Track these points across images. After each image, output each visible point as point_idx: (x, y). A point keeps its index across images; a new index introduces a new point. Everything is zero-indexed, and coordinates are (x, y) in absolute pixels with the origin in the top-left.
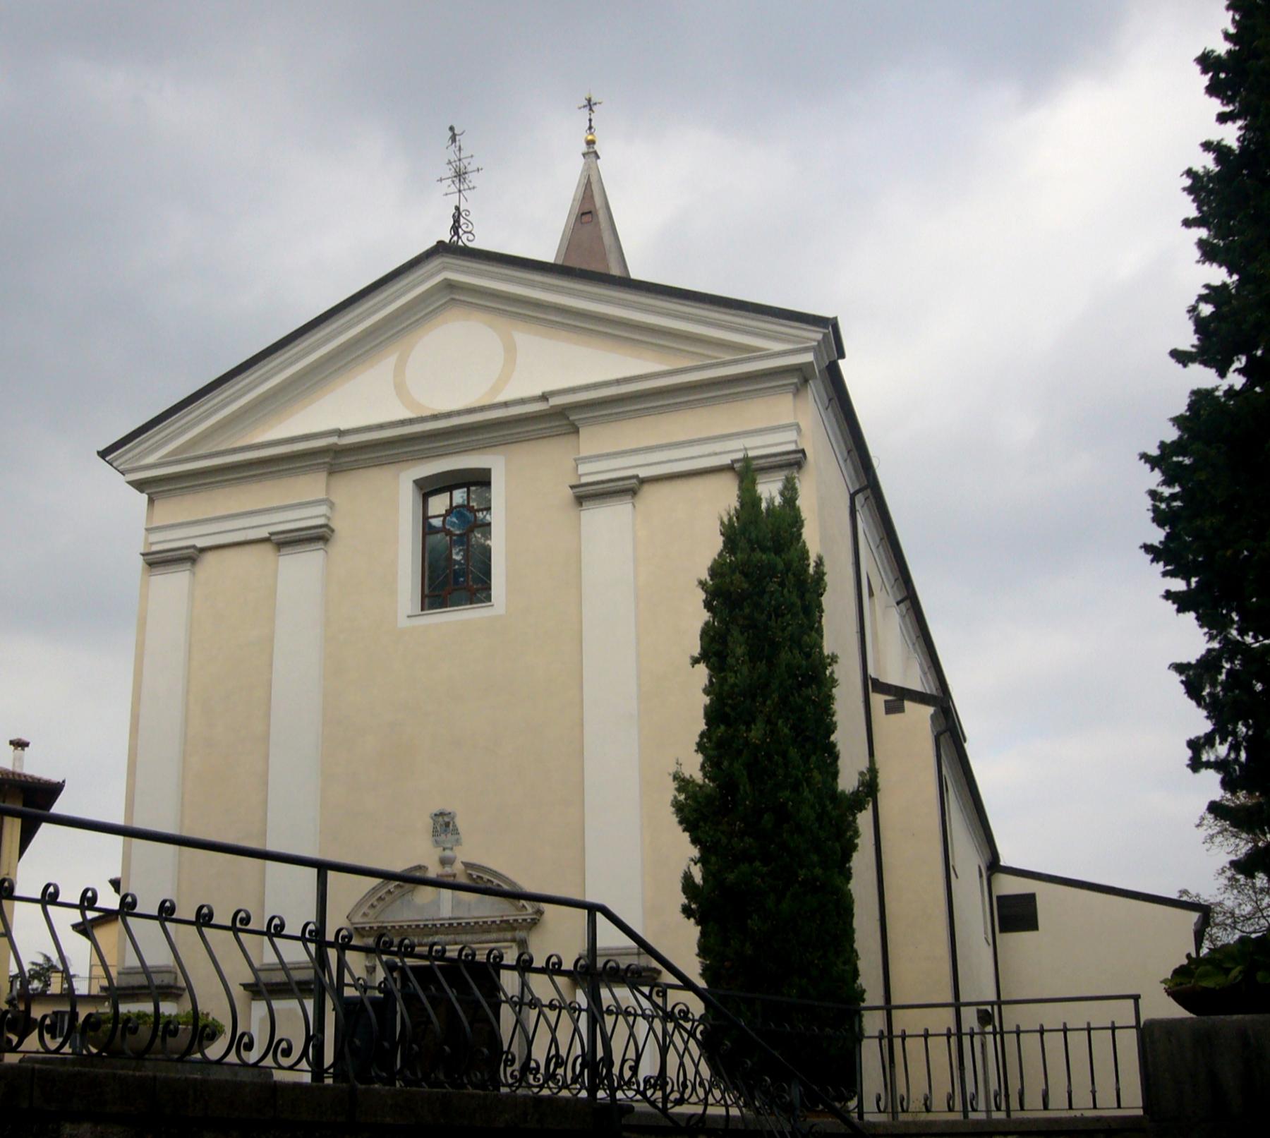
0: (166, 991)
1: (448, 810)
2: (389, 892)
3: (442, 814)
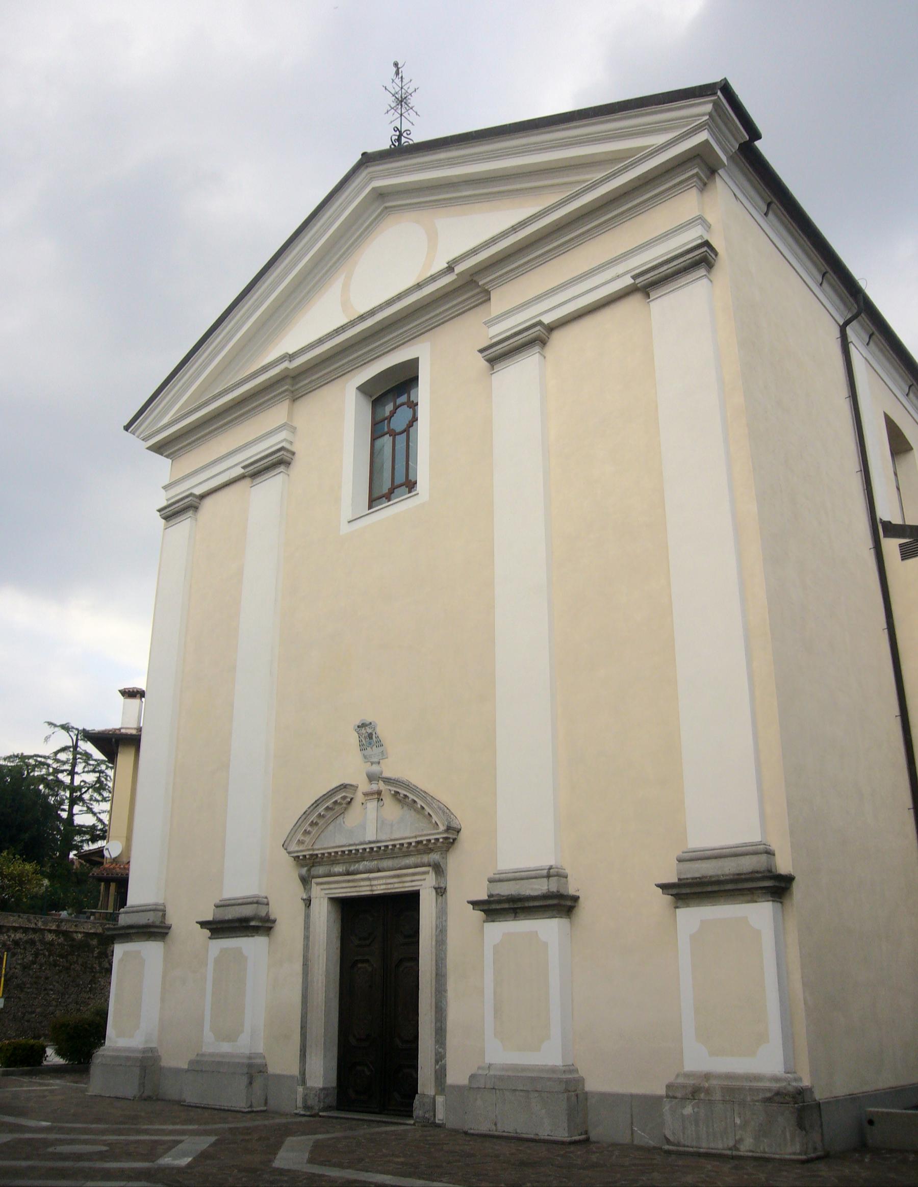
0: (145, 930)
1: (368, 720)
2: (320, 816)
3: (363, 725)
